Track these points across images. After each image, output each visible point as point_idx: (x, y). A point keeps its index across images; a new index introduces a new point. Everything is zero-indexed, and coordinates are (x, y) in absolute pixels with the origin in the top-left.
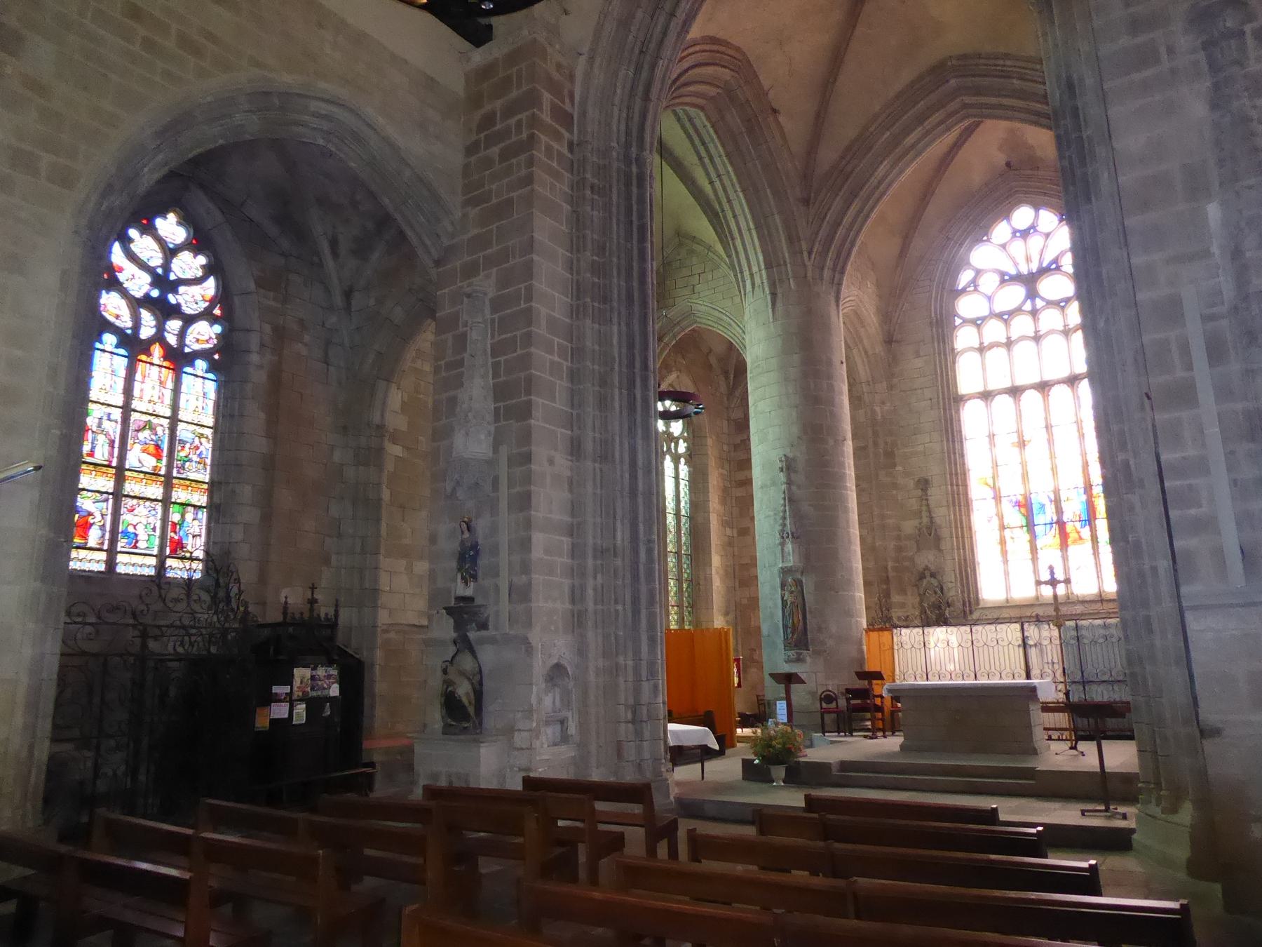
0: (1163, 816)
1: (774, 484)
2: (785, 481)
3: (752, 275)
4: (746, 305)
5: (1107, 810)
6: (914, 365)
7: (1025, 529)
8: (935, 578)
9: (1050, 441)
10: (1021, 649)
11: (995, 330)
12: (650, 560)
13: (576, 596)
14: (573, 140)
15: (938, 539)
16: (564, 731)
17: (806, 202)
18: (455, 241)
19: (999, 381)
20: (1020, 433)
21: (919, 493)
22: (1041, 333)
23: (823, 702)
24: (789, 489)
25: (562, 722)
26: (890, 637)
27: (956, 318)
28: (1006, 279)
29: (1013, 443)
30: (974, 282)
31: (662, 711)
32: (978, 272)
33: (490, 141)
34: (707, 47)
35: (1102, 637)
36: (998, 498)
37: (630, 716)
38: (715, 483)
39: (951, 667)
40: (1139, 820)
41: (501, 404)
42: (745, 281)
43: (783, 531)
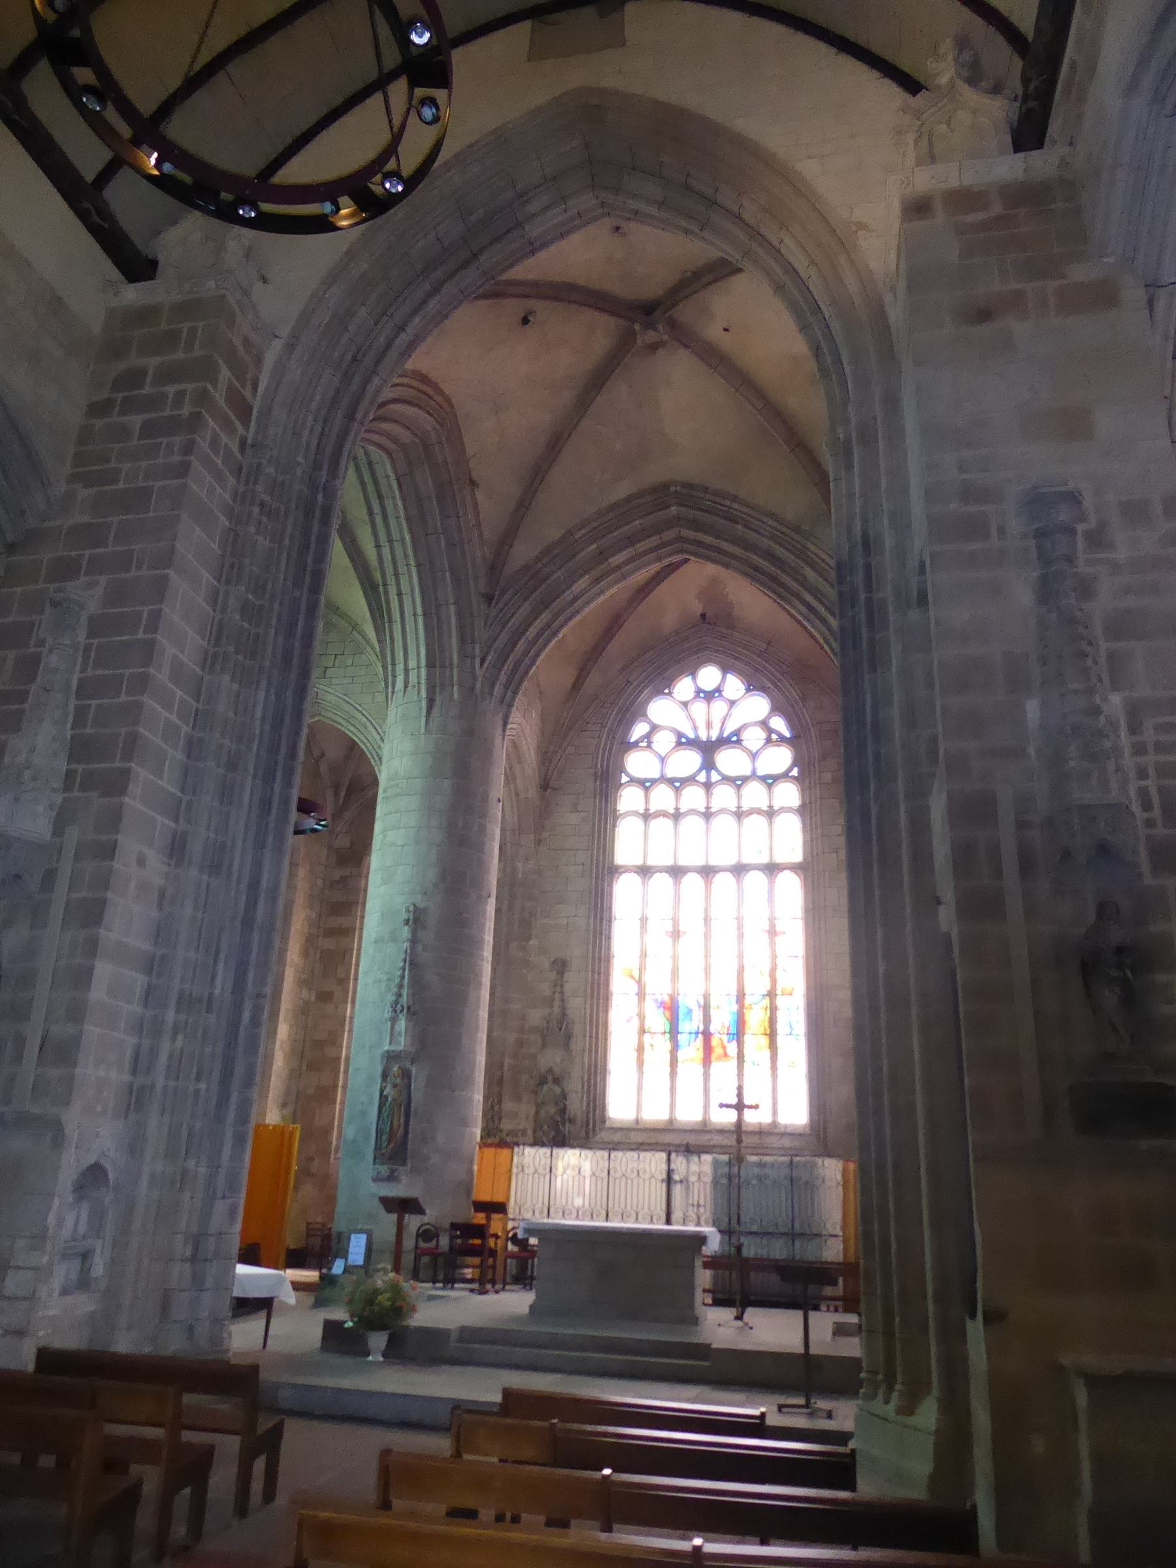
0: (899, 1418)
1: (394, 938)
3: (406, 670)
4: (392, 707)
5: (807, 1406)
6: (568, 819)
7: (668, 1035)
9: (707, 936)
10: (664, 1185)
11: (662, 797)
12: (256, 1022)
13: (140, 1063)
14: (246, 438)
15: (569, 1037)
16: (85, 1270)
17: (489, 598)
18: (47, 524)
19: (659, 857)
20: (675, 921)
21: (553, 976)
22: (713, 810)
23: (420, 1239)
25: (86, 1256)
27: (623, 774)
28: (683, 742)
29: (666, 932)
30: (648, 737)
31: (235, 1246)
32: (654, 728)
33: (129, 406)
34: (415, 383)
36: (641, 995)
37: (189, 1252)
38: (299, 927)
39: (578, 1202)
40: (858, 1420)
41: (80, 767)
43: (396, 1002)
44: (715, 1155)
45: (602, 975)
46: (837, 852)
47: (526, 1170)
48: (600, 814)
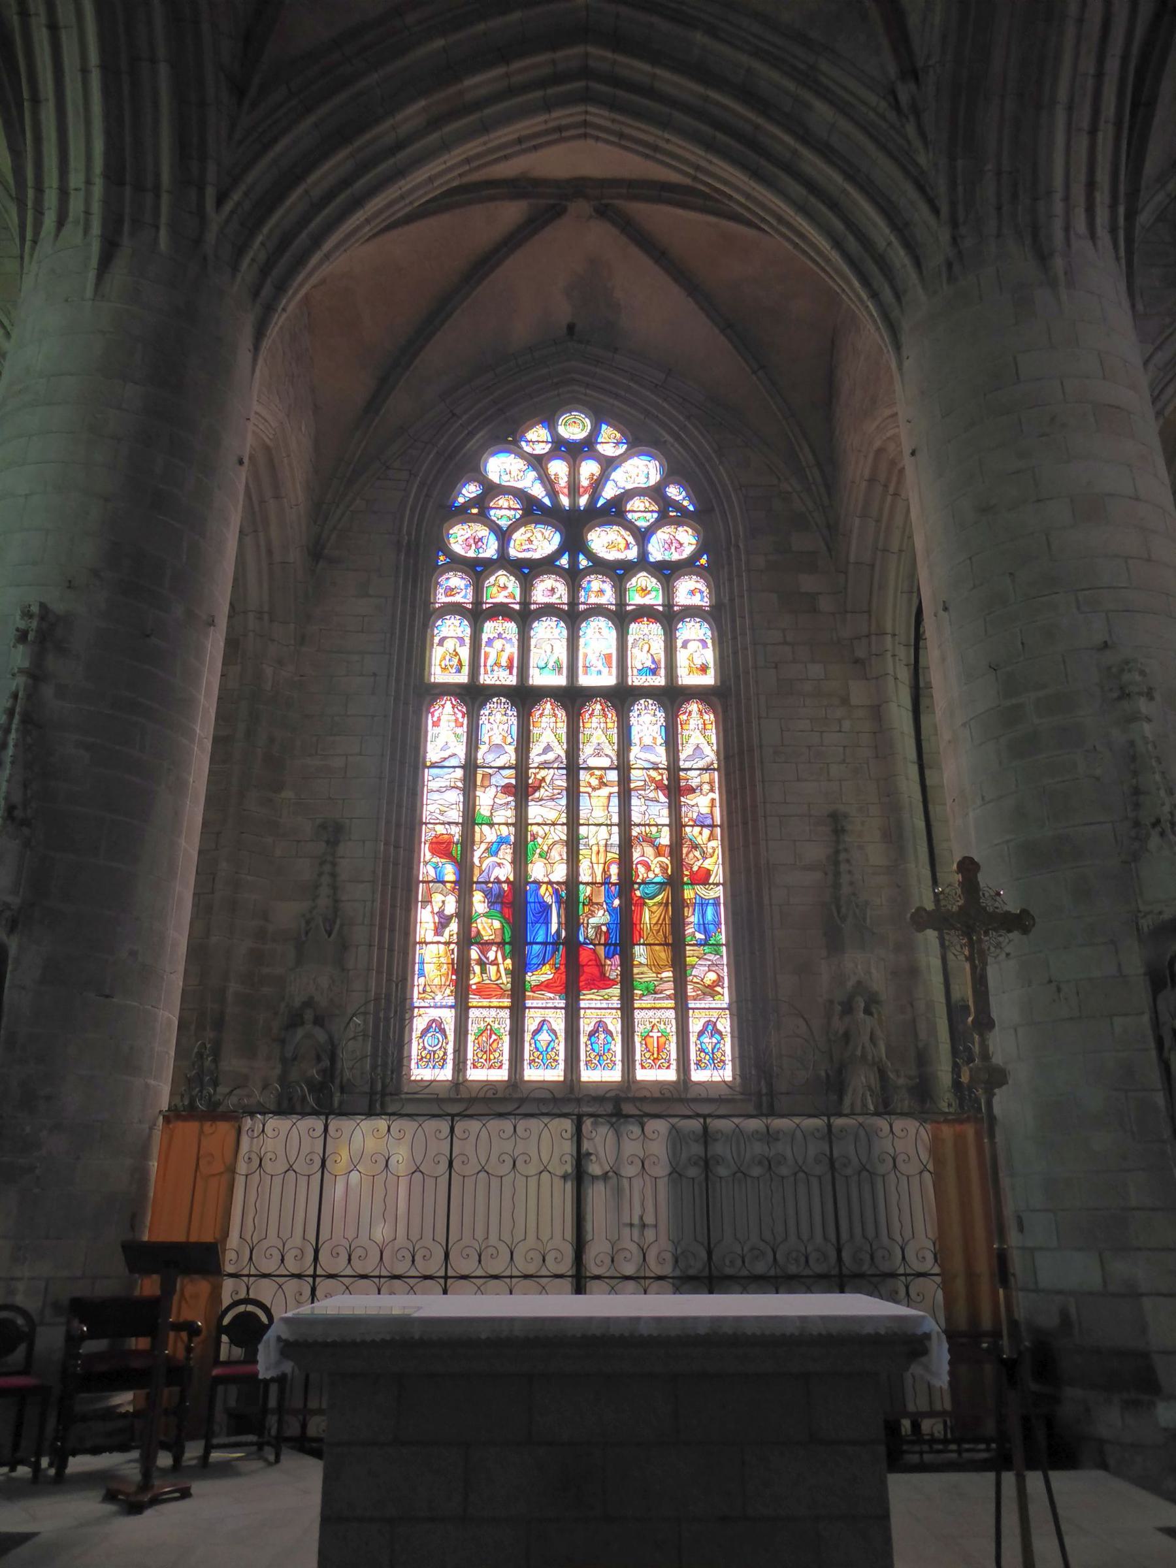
2: (26, 664)
3: (64, 193)
8: (322, 1026)
15: (344, 946)
24: (32, 694)
26: (233, 1133)
28: (532, 511)
35: (760, 1163)
36: (464, 886)
42: (42, 214)
44: (674, 1120)
45: (400, 867)
46: (776, 667)
47: (267, 1165)
48: (404, 602)
